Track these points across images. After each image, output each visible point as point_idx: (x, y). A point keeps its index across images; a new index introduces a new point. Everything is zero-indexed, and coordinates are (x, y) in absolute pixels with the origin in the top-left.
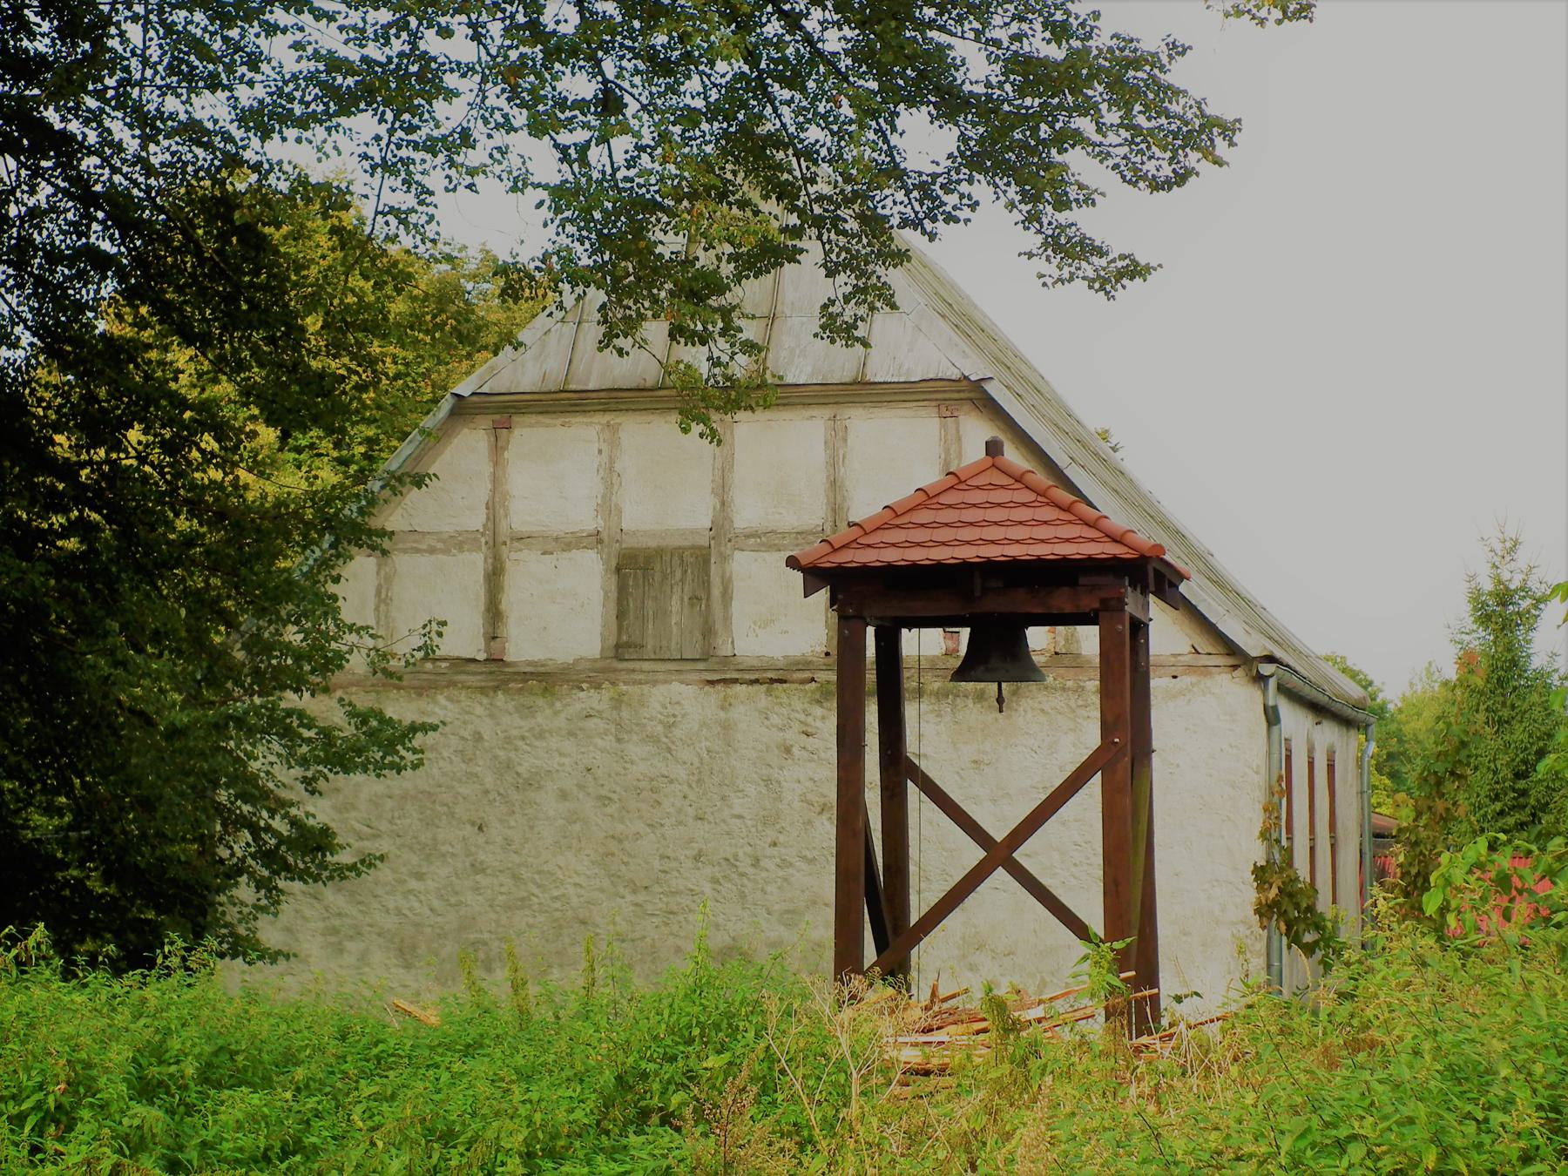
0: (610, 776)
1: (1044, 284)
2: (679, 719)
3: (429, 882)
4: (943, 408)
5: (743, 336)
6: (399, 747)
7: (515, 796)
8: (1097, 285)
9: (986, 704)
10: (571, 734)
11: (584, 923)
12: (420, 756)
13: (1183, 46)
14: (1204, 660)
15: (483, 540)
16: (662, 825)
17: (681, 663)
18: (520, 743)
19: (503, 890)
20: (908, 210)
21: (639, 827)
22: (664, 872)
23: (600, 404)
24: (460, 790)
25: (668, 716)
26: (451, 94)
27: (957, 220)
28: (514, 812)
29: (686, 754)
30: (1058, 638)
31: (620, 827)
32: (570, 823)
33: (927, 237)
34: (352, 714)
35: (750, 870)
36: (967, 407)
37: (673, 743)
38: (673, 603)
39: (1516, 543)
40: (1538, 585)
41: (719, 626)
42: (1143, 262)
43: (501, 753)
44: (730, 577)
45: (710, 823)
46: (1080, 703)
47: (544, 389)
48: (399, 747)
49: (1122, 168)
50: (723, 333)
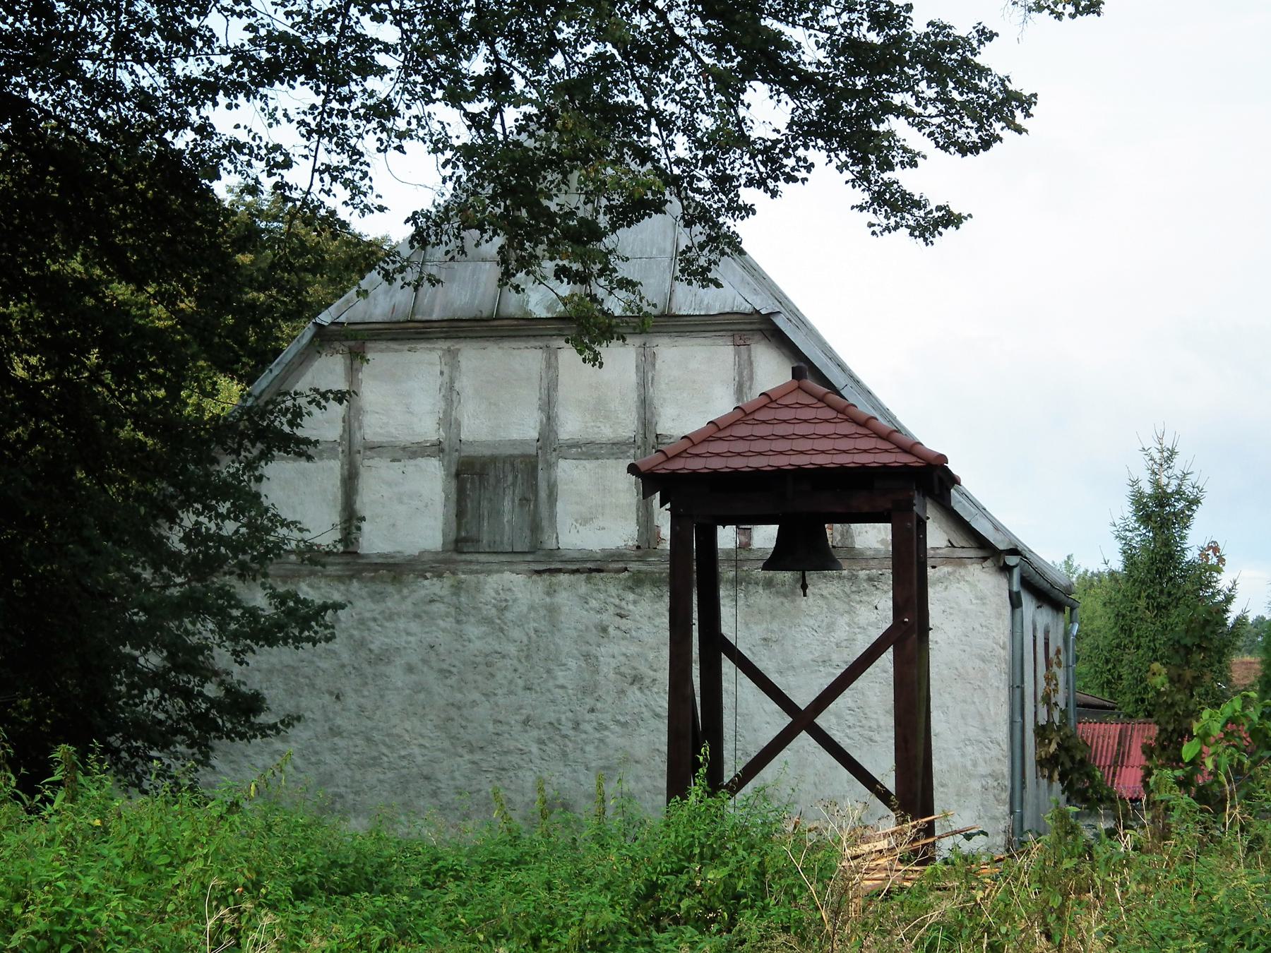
0: (450, 653)
1: (874, 233)
2: (510, 603)
3: (293, 744)
4: (737, 338)
5: (619, 275)
6: (313, 623)
7: (368, 670)
8: (917, 233)
9: (773, 590)
10: (417, 616)
11: (427, 778)
12: (331, 630)
13: (991, 32)
14: (959, 553)
15: (340, 449)
16: (495, 694)
17: (513, 555)
18: (372, 624)
19: (357, 750)
20: (754, 171)
21: (476, 696)
22: (497, 734)
23: (441, 332)
24: (319, 664)
25: (501, 601)
26: (382, 71)
27: (795, 180)
28: (366, 683)
29: (516, 633)
30: (835, 534)
31: (459, 696)
32: (416, 693)
33: (769, 194)
34: (273, 596)
35: (571, 733)
36: (757, 337)
37: (505, 624)
38: (506, 503)
39: (1173, 453)
40: (1191, 489)
41: (545, 523)
42: (956, 212)
43: (356, 633)
44: (556, 481)
45: (536, 692)
46: (854, 589)
47: (394, 320)
48: (313, 623)
49: (937, 135)
50: (601, 273)
